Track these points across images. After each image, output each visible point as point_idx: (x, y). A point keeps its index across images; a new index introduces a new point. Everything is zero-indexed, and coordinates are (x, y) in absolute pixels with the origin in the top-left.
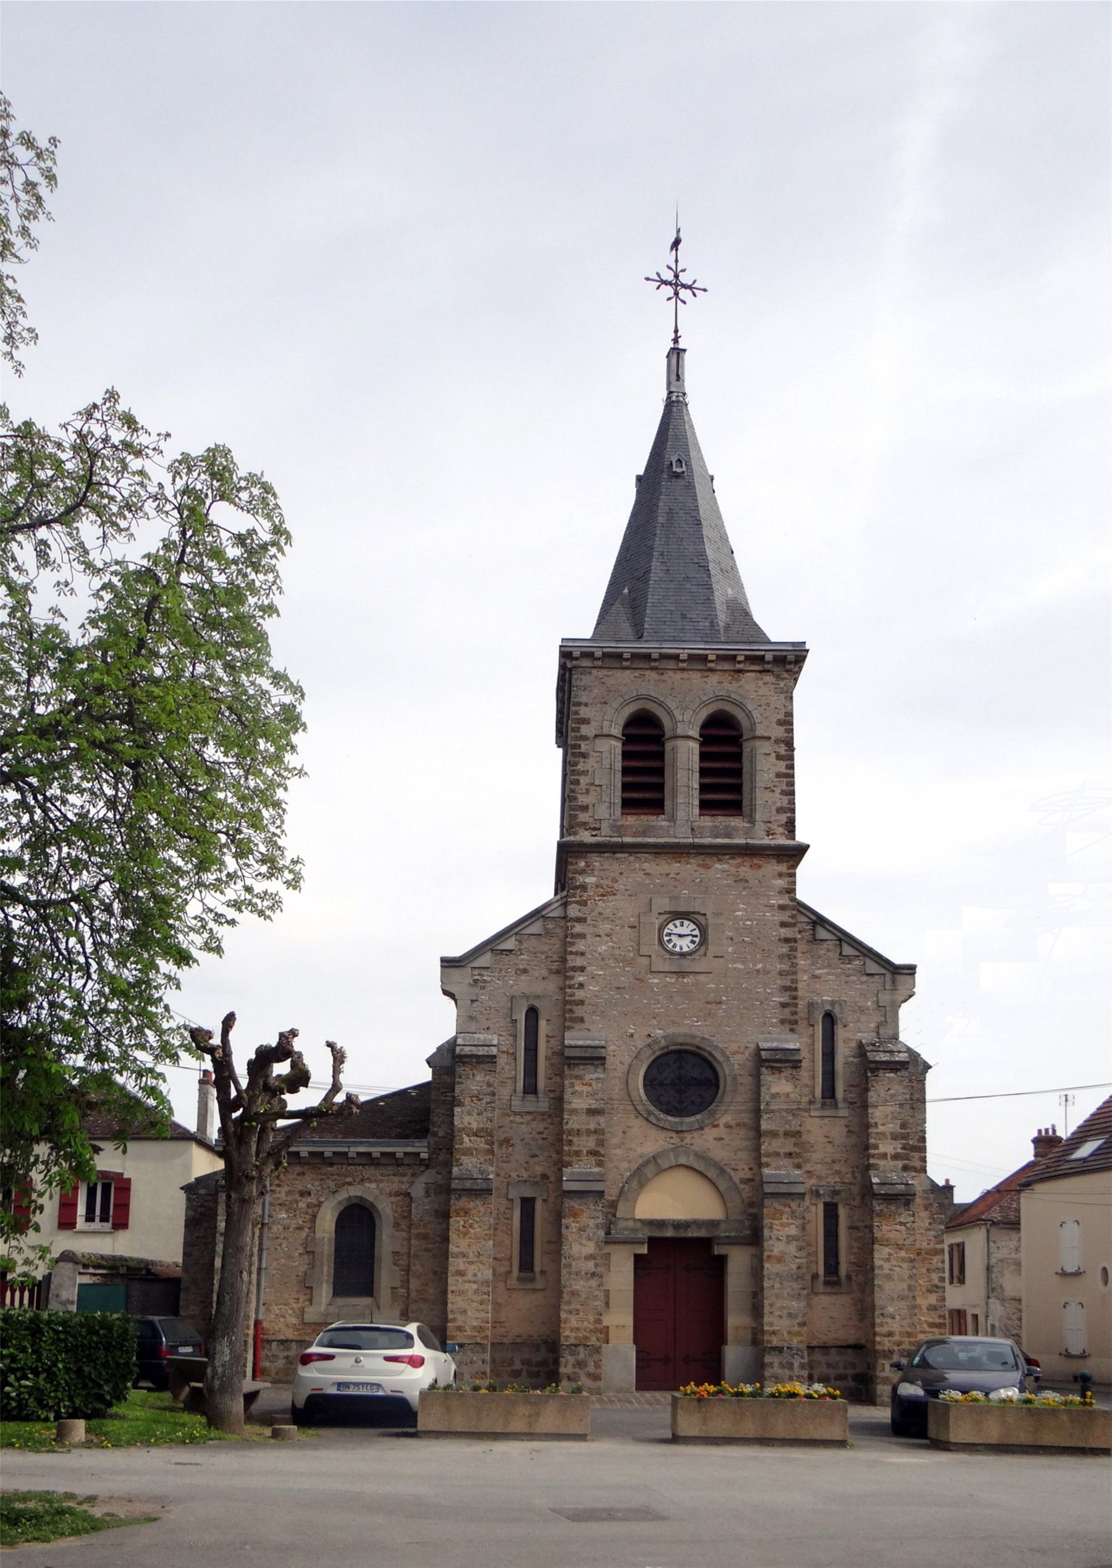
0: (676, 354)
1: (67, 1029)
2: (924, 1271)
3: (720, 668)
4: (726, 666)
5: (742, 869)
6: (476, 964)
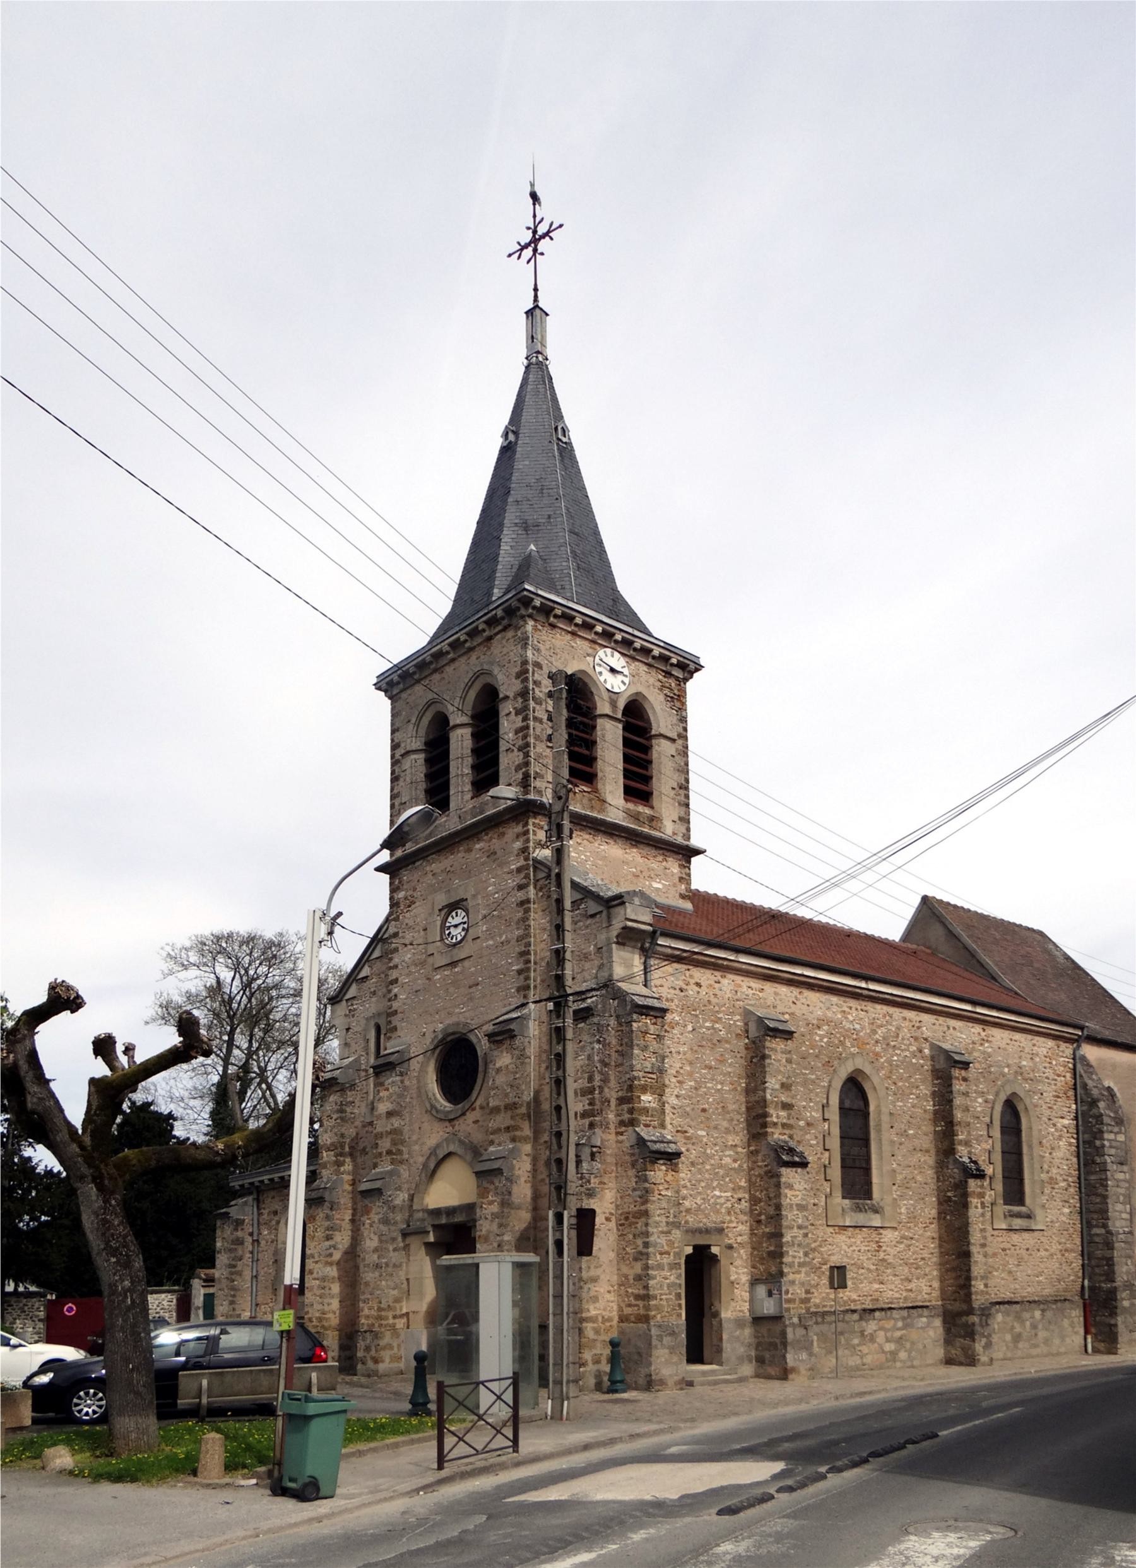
0: (535, 313)
2: (631, 1236)
3: (475, 644)
4: (479, 640)
6: (347, 997)
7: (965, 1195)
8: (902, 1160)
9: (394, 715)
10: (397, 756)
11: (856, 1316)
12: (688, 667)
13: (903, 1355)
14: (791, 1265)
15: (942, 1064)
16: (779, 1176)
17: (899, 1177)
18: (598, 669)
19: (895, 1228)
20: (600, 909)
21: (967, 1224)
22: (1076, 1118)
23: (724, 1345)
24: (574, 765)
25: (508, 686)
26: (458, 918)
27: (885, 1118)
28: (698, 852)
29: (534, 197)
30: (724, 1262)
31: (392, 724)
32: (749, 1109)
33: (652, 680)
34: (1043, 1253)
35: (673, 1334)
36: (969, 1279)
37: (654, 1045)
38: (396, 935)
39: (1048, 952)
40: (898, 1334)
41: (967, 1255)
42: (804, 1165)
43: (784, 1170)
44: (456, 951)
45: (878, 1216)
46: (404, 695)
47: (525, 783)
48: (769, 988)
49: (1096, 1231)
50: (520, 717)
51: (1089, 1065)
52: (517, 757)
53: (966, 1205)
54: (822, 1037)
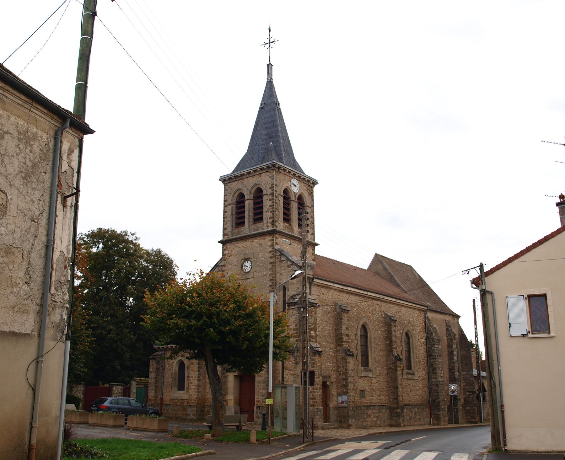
0: (269, 66)
7: (396, 367)
8: (376, 354)
10: (226, 204)
11: (365, 408)
12: (315, 183)
13: (378, 422)
14: (350, 389)
16: (347, 359)
17: (377, 360)
21: (397, 377)
23: (331, 416)
24: (286, 217)
25: (267, 191)
26: (248, 264)
27: (373, 339)
28: (317, 245)
29: (270, 29)
30: (330, 387)
32: (336, 336)
33: (305, 188)
34: (417, 388)
36: (397, 396)
37: (314, 315)
38: (224, 266)
39: (414, 275)
40: (377, 415)
41: (397, 388)
42: (353, 355)
43: (348, 357)
44: (247, 275)
46: (229, 184)
47: (273, 223)
48: (341, 294)
50: (271, 202)
52: (270, 214)
53: (396, 370)
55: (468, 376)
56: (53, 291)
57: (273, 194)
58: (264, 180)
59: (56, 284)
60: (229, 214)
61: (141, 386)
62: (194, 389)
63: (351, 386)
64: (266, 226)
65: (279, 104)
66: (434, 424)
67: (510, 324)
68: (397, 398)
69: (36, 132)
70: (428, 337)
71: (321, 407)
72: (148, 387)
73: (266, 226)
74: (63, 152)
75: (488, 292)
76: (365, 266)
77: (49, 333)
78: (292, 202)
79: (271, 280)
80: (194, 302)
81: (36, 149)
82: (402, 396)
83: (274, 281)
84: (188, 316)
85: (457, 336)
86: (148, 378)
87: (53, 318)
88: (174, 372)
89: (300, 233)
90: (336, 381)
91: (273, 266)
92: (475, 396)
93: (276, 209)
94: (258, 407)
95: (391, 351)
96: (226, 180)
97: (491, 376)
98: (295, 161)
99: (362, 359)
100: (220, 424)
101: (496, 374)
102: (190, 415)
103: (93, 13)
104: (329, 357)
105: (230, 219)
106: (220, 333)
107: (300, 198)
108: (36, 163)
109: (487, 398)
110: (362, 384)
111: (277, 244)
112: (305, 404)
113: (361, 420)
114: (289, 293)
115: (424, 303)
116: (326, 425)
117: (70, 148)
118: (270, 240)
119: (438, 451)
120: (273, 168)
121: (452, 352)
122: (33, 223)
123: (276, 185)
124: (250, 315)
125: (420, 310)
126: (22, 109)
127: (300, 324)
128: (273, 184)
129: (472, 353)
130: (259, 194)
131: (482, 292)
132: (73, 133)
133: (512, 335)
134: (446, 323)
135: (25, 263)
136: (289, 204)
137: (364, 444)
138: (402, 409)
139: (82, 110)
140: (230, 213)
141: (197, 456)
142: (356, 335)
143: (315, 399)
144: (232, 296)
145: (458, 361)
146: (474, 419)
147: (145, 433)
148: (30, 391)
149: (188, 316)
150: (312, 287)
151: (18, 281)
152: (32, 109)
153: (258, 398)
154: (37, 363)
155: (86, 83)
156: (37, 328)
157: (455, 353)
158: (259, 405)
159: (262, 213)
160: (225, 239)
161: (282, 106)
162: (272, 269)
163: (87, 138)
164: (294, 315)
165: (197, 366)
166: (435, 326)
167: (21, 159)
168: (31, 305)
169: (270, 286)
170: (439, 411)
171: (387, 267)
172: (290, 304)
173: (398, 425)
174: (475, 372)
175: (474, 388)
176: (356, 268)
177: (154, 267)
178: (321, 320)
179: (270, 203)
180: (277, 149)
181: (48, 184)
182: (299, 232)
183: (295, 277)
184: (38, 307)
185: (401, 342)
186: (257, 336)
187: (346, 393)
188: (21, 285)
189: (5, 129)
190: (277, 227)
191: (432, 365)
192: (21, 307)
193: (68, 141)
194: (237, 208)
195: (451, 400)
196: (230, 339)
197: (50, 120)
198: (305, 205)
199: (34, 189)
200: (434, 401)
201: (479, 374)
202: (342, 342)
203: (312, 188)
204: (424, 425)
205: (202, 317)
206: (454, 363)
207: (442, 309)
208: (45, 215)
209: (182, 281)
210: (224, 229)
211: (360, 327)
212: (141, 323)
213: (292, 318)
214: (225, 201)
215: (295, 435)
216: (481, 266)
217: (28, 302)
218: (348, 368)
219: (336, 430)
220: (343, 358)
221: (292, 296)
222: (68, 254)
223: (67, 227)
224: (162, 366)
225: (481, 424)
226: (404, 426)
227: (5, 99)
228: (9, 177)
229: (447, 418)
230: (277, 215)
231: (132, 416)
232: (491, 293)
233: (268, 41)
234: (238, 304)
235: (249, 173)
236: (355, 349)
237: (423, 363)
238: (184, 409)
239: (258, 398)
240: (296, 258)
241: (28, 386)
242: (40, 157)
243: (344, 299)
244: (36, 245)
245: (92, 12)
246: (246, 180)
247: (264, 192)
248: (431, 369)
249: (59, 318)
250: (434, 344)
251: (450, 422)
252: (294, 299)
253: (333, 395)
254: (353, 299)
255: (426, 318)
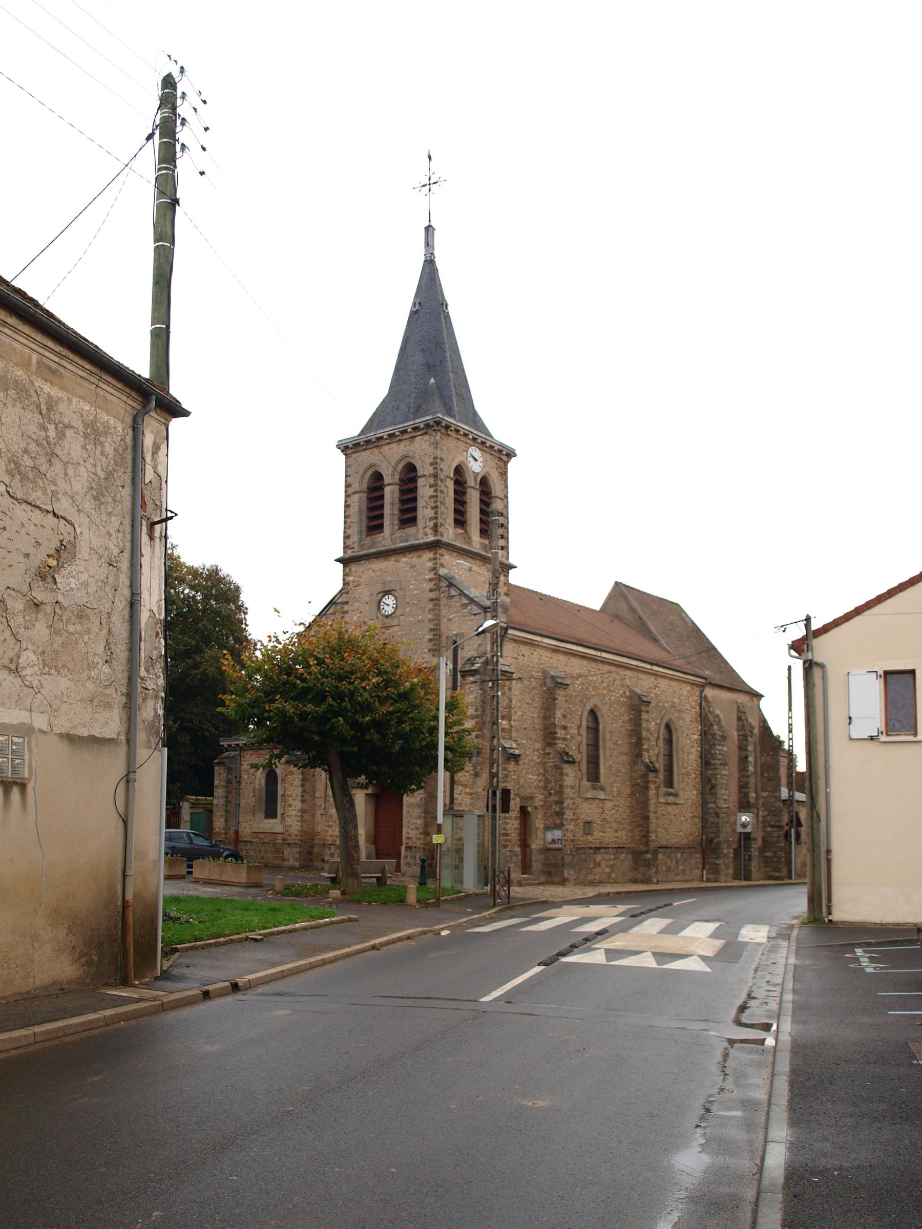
0: (429, 230)
1: (685, 860)
4: (406, 436)
5: (414, 559)
7: (647, 782)
8: (614, 759)
9: (348, 466)
11: (592, 851)
12: (510, 454)
13: (613, 875)
14: (567, 820)
15: (636, 702)
16: (562, 769)
17: (614, 770)
18: (469, 459)
19: (610, 800)
20: (480, 611)
21: (648, 799)
22: (701, 735)
24: (459, 517)
25: (424, 469)
26: (390, 601)
28: (513, 567)
29: (430, 157)
30: (533, 816)
31: (346, 472)
32: (545, 728)
34: (683, 818)
35: (516, 855)
36: (648, 832)
38: (347, 603)
40: (612, 862)
41: (647, 818)
42: (573, 762)
43: (565, 766)
45: (603, 792)
46: (354, 456)
48: (555, 656)
49: (710, 805)
50: (432, 490)
51: (708, 702)
53: (647, 788)
54: (579, 685)
55: (772, 799)
56: (143, 673)
57: (435, 476)
58: (420, 450)
59: (146, 661)
60: (354, 509)
61: (198, 811)
62: (296, 816)
63: (569, 814)
64: (421, 533)
65: (447, 306)
66: (708, 880)
67: (850, 718)
68: (646, 836)
69: (107, 421)
70: (705, 732)
71: (518, 849)
72: (212, 811)
73: (421, 533)
74: (145, 451)
75: (817, 664)
76: (598, 609)
77: (141, 736)
78: (469, 490)
79: (431, 630)
80: (310, 674)
81: (109, 449)
82: (656, 832)
83: (436, 631)
84: (302, 695)
85: (756, 731)
86: (212, 795)
87: (144, 714)
88: (257, 786)
89: (484, 547)
90: (543, 806)
91: (435, 605)
92: (782, 833)
93: (441, 502)
94: (408, 848)
95: (639, 755)
96: (349, 448)
97: (813, 802)
98: (475, 413)
99: (588, 768)
100: (355, 875)
101: (821, 800)
102: (288, 860)
103: (172, 200)
104: (532, 764)
105: (356, 520)
106: (355, 725)
107: (484, 482)
108: (110, 472)
109: (804, 837)
110: (588, 811)
111: (442, 565)
112: (494, 844)
113: (584, 872)
114: (464, 655)
115: (701, 673)
116: (526, 879)
117: (154, 443)
118: (430, 560)
119: (718, 920)
120: (435, 428)
121: (746, 757)
122: (111, 568)
123: (442, 459)
124: (405, 696)
125: (692, 684)
126: (86, 384)
127: (482, 707)
128: (435, 458)
129: (782, 759)
130: (409, 475)
131: (807, 665)
132: (158, 418)
133: (853, 736)
134: (738, 707)
135: (104, 632)
136: (464, 493)
137: (594, 909)
138: (655, 853)
139: (165, 374)
140: (357, 509)
141: (332, 923)
142: (579, 727)
143: (507, 835)
144: (375, 662)
145: (755, 773)
146: (779, 872)
147: (227, 888)
148: (120, 824)
149: (302, 695)
150: (504, 643)
151: (97, 659)
152: (101, 384)
153: (408, 833)
154: (128, 781)
155: (168, 327)
156: (123, 729)
157: (751, 759)
158: (410, 844)
159: (415, 509)
160: (347, 556)
161: (451, 310)
162: (433, 610)
163: (176, 424)
164: (472, 692)
165: (301, 777)
166: (718, 712)
167: (89, 467)
168: (114, 696)
169: (430, 640)
170: (717, 858)
171: (636, 606)
172: (465, 674)
173: (648, 881)
174: (784, 793)
175: (780, 820)
176: (580, 609)
177: (206, 598)
178: (521, 704)
179: (431, 492)
180: (441, 388)
181: (127, 503)
182: (481, 544)
183: (483, 632)
184: (124, 698)
185: (658, 739)
186: (417, 731)
187: (560, 826)
188: (100, 665)
189: (66, 421)
190: (442, 535)
191: (710, 780)
192: (102, 699)
193: (152, 432)
194: (370, 500)
195: (740, 839)
196: (373, 735)
197: (125, 398)
198: (493, 494)
199: (110, 514)
200: (710, 841)
201: (791, 796)
202: (554, 739)
203: (506, 463)
204: (692, 880)
205: (325, 698)
206: (748, 777)
207: (733, 684)
208: (127, 555)
209: (287, 636)
210: (346, 537)
211: (586, 714)
212: (219, 710)
213: (470, 695)
214: (347, 486)
215: (476, 894)
216: (808, 619)
217: (111, 691)
218: (565, 784)
219: (542, 887)
220: (555, 766)
221: (469, 659)
222: (160, 614)
223: (157, 572)
224: (236, 777)
225: (789, 881)
226: (658, 882)
227: (62, 371)
228: (77, 497)
229: (731, 871)
230: (442, 513)
231: (201, 860)
232: (821, 666)
233: (426, 182)
234: (385, 677)
235: (391, 436)
236: (576, 752)
237: (693, 776)
238: (278, 850)
239: (408, 833)
240: (479, 592)
241: (117, 816)
242: (115, 461)
243: (562, 666)
244: (117, 603)
245: (171, 199)
246: (386, 448)
247: (420, 472)
248: (708, 787)
249: (152, 713)
250: (714, 744)
251: (736, 877)
252: (473, 664)
253: (537, 828)
254: (576, 666)
255: (703, 698)
